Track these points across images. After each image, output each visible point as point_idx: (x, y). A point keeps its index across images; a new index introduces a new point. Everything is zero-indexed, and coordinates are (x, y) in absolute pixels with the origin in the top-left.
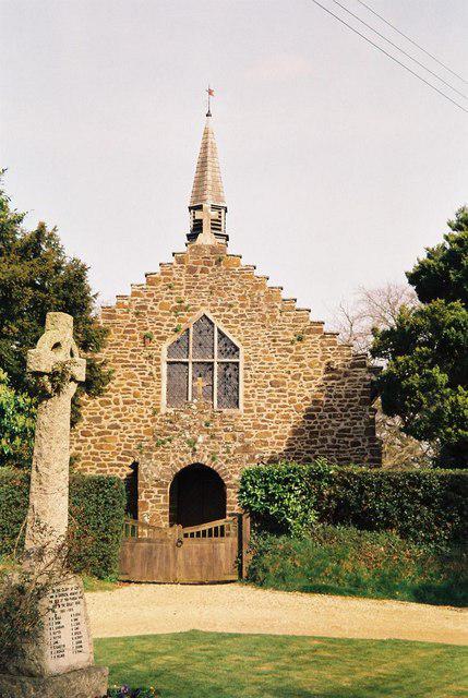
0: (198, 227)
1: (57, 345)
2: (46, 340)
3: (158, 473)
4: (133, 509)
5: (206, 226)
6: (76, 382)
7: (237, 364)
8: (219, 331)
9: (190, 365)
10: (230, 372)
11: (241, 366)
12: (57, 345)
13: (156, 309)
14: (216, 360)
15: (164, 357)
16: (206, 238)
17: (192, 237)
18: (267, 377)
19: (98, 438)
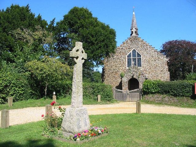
0: (132, 33)
1: (77, 51)
2: (74, 49)
3: (125, 80)
4: (97, 100)
5: (134, 32)
6: (84, 59)
7: (141, 59)
8: (137, 52)
9: (132, 59)
10: (139, 60)
11: (142, 59)
12: (77, 51)
13: (125, 49)
14: (137, 58)
15: (127, 58)
16: (134, 34)
17: (131, 35)
18: (147, 61)
19: (115, 73)
